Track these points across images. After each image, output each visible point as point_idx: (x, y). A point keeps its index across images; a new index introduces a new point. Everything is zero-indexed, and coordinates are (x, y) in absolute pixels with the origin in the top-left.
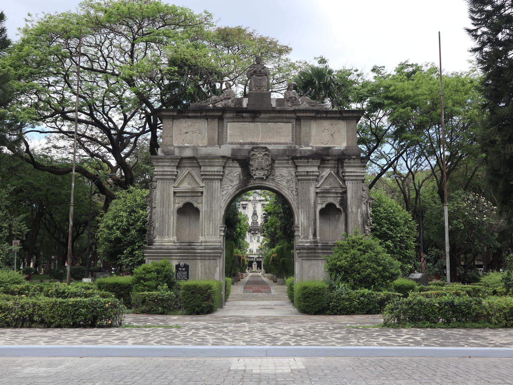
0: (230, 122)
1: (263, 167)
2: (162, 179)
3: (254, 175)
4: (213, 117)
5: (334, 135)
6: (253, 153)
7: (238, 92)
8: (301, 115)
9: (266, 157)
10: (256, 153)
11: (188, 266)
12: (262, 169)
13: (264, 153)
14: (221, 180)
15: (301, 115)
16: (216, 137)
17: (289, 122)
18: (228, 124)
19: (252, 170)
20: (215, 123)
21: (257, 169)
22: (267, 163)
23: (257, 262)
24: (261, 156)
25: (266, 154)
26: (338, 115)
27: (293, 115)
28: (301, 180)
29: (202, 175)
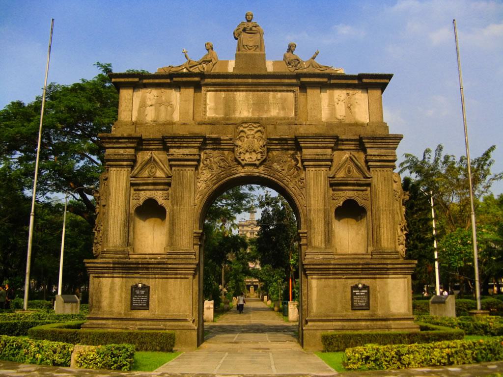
0: (210, 91)
1: (255, 148)
2: (315, 166)
3: (243, 160)
4: (187, 85)
5: (351, 107)
6: (241, 129)
7: (218, 267)
8: (308, 80)
9: (259, 134)
10: (245, 130)
11: (149, 288)
12: (254, 151)
13: (256, 130)
14: (197, 167)
15: (308, 80)
16: (191, 111)
17: (291, 91)
18: (209, 94)
19: (240, 153)
20: (190, 92)
21: (247, 151)
22: (261, 143)
23: (254, 286)
24: (253, 132)
25: (259, 131)
26: (356, 82)
27: (294, 81)
28: (175, 166)
29: (369, 185)
